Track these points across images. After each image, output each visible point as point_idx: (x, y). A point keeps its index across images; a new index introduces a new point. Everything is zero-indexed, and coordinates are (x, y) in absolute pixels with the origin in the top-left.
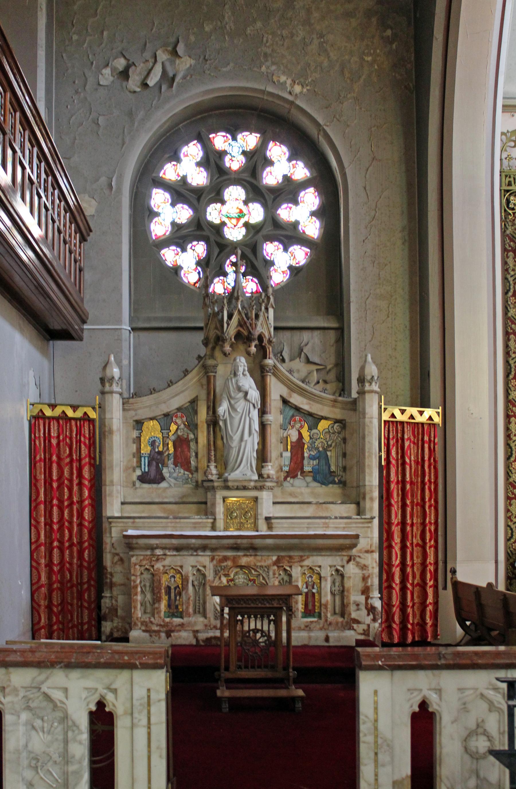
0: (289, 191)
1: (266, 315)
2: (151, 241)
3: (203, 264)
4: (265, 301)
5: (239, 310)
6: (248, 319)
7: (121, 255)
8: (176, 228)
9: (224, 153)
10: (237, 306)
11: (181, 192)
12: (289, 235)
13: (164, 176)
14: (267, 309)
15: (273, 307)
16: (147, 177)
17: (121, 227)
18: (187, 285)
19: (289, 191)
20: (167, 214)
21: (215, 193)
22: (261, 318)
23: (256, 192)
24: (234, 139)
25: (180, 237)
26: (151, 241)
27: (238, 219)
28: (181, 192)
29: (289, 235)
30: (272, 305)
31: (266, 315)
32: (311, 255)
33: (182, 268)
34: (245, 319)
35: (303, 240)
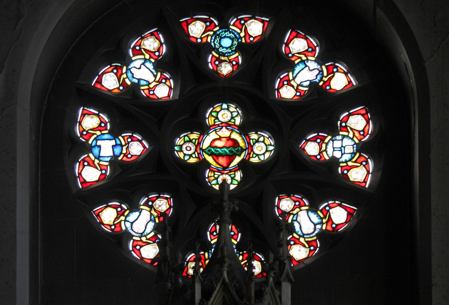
0: (321, 111)
1: (277, 293)
2: (74, 192)
3: (165, 228)
4: (276, 267)
5: (224, 281)
6: (242, 299)
7: (15, 206)
8: (119, 170)
9: (206, 48)
10: (222, 275)
11: (128, 111)
12: (322, 183)
13: (98, 86)
14: (278, 284)
15: (290, 281)
16: (68, 86)
17: (14, 158)
18: (140, 263)
19: (321, 111)
20: (105, 148)
21: (188, 114)
22: (267, 298)
23: (261, 112)
24: (225, 26)
25: (126, 184)
26: (74, 192)
27: (231, 158)
28: (128, 111)
29: (322, 183)
30: (288, 275)
31: (277, 293)
32: (358, 215)
33: (131, 236)
34: (237, 297)
35: (346, 192)
